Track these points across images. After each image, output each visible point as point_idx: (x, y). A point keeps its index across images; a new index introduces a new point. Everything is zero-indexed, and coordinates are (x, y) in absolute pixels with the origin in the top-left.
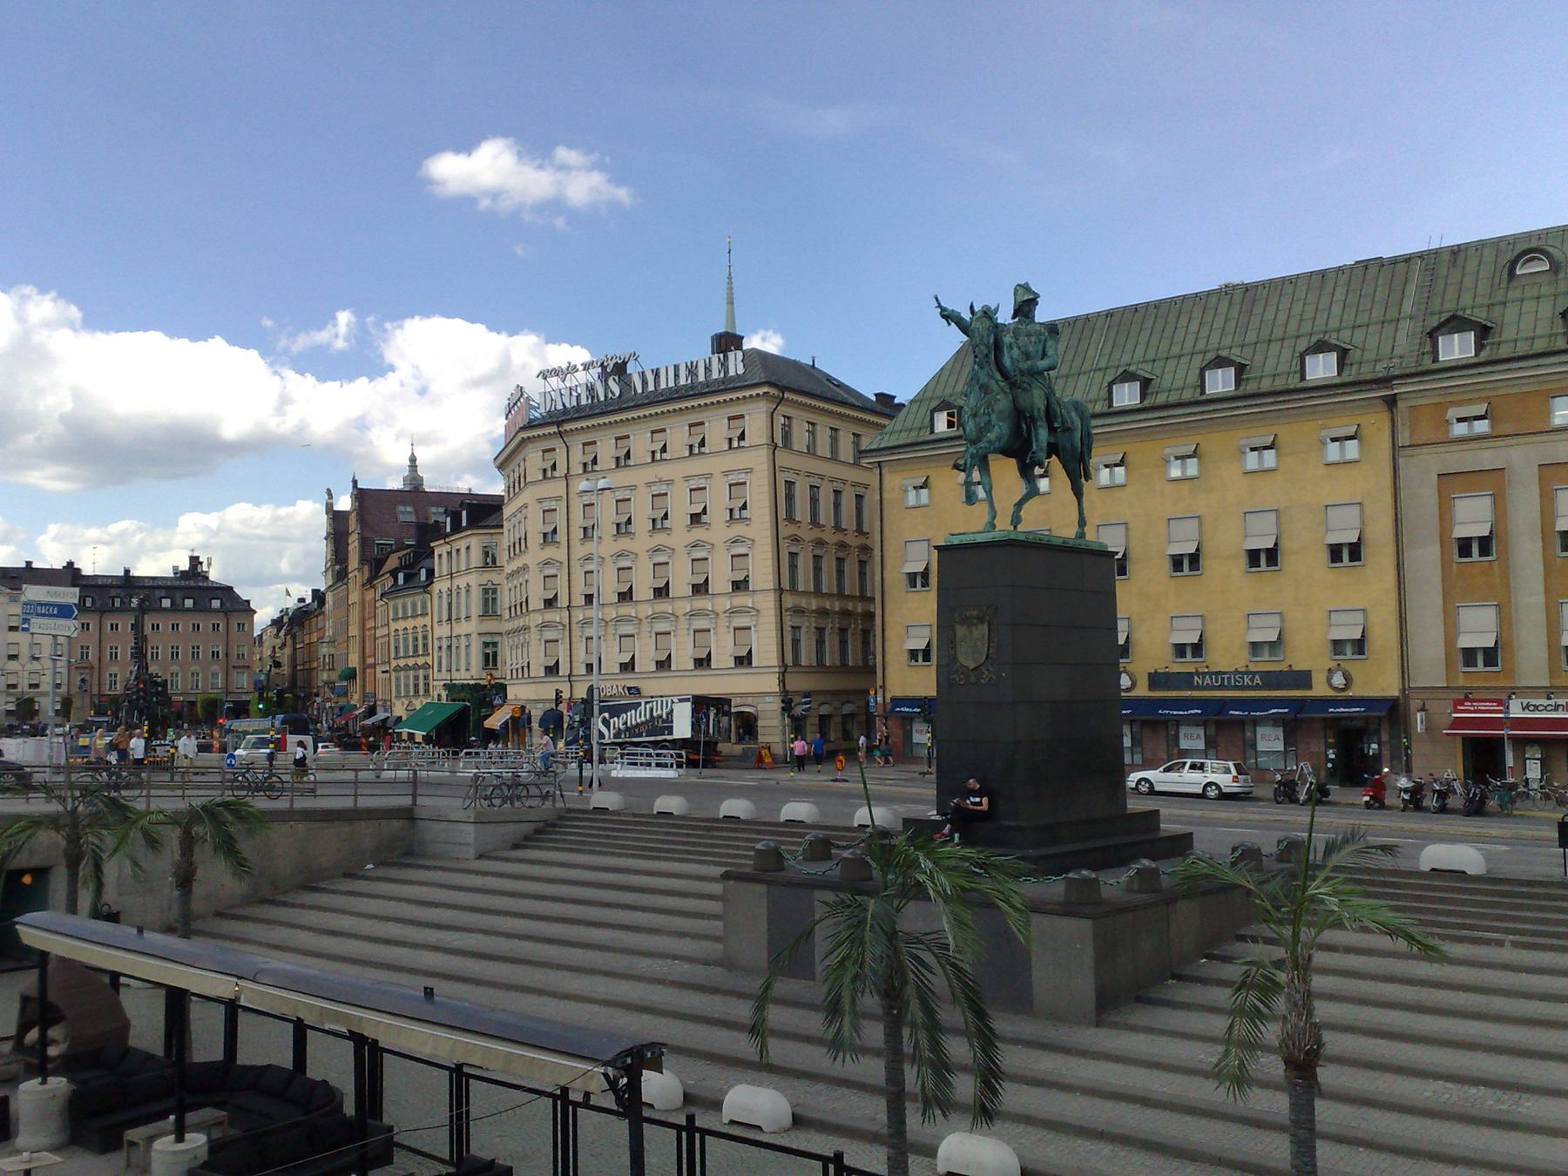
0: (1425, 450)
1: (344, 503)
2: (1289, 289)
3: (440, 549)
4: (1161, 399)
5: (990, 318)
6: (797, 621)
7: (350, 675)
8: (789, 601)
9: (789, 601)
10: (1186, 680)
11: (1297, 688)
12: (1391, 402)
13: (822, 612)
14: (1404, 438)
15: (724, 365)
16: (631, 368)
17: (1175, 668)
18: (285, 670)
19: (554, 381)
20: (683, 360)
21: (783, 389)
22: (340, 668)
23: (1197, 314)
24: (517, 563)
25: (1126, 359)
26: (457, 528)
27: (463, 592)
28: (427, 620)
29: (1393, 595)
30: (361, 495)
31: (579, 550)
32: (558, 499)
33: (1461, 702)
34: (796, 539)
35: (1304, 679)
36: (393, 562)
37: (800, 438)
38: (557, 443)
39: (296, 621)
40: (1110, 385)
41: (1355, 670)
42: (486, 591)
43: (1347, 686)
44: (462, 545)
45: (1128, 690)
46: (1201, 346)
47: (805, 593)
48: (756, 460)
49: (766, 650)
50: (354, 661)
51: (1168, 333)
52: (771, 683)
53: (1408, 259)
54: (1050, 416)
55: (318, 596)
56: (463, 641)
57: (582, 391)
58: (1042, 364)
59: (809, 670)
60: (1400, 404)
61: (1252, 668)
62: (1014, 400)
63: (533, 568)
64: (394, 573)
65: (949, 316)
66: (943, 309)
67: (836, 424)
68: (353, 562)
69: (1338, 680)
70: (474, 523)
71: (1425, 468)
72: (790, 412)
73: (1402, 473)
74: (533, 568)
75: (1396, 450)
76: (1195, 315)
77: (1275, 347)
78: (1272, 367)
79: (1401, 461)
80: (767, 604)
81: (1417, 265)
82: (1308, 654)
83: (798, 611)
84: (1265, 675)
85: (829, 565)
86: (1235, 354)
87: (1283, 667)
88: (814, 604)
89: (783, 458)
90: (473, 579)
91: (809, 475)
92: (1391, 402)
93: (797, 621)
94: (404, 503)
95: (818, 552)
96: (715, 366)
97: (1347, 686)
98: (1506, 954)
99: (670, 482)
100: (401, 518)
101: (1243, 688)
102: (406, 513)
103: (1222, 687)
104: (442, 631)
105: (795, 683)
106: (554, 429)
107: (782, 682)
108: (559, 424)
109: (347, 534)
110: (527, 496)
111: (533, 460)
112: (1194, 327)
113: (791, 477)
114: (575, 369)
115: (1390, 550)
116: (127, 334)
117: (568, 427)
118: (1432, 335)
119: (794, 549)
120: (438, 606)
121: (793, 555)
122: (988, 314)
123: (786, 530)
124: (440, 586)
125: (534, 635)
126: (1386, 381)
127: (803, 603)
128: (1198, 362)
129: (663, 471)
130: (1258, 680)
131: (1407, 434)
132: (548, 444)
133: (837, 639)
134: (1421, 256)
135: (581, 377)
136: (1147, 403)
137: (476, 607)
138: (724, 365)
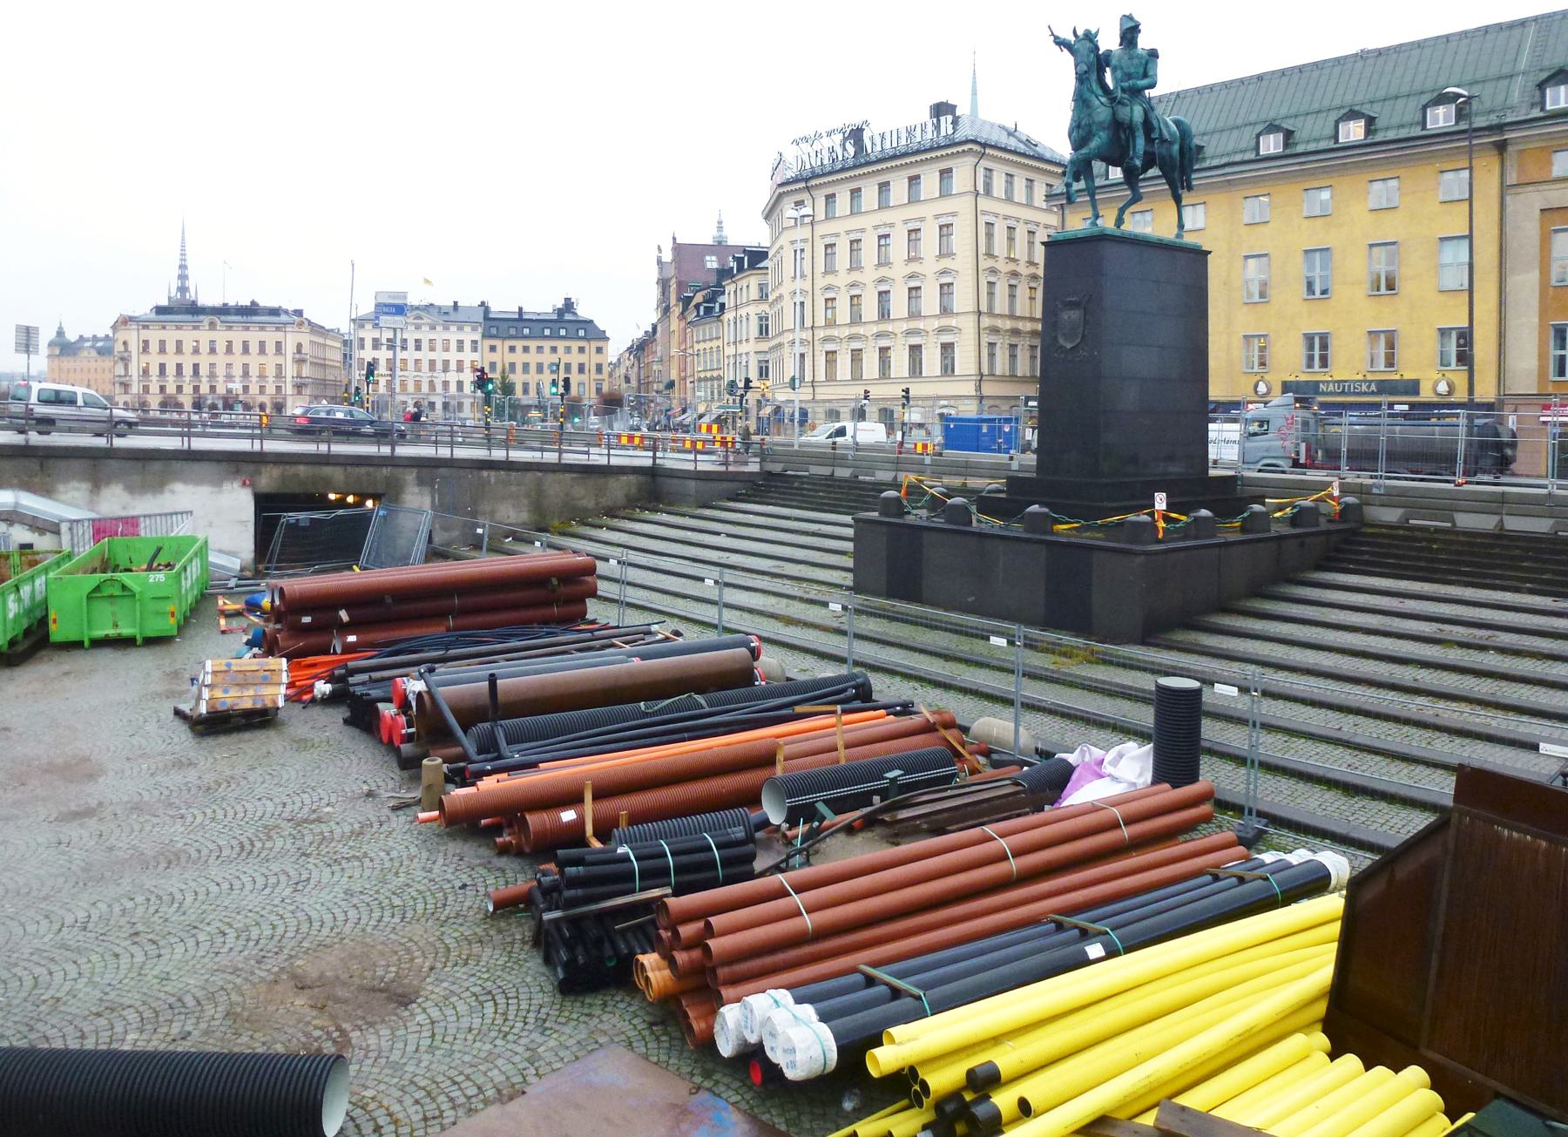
0: (1530, 188)
1: (667, 256)
2: (1416, 52)
3: (730, 288)
4: (1300, 149)
5: (1091, 41)
6: (992, 339)
7: (671, 385)
8: (986, 322)
9: (986, 322)
12: (1501, 147)
13: (1015, 332)
14: (1512, 178)
15: (937, 127)
16: (866, 135)
17: (1303, 378)
18: (634, 383)
19: (805, 147)
20: (902, 124)
21: (984, 145)
22: (666, 381)
24: (776, 294)
26: (741, 269)
28: (720, 343)
29: (1495, 315)
30: (678, 248)
31: (821, 282)
32: (804, 241)
34: (993, 271)
36: (699, 298)
37: (1020, 193)
38: (805, 196)
39: (640, 348)
40: (1258, 137)
42: (761, 319)
44: (744, 283)
46: (1337, 102)
47: (1001, 316)
48: (962, 206)
49: (965, 361)
50: (674, 375)
52: (969, 389)
53: (1523, 23)
54: (1148, 125)
55: (655, 328)
56: (744, 359)
57: (826, 154)
58: (1141, 83)
59: (1002, 379)
60: (1510, 149)
61: (1369, 377)
62: (1114, 114)
63: (787, 297)
64: (697, 307)
65: (1060, 43)
66: (1056, 38)
67: (1031, 176)
68: (673, 301)
70: (752, 266)
71: (1527, 206)
72: (990, 165)
73: (1509, 210)
74: (787, 297)
75: (1504, 189)
78: (1396, 119)
79: (1508, 199)
80: (968, 325)
81: (1532, 29)
83: (995, 330)
84: (1380, 383)
85: (1001, 290)
86: (1366, 110)
87: (1397, 377)
88: (1008, 324)
89: (984, 204)
90: (753, 310)
91: (1006, 218)
92: (1501, 147)
93: (992, 339)
94: (712, 254)
95: (1013, 282)
96: (930, 128)
97: (1450, 393)
98: (664, 517)
99: (892, 225)
100: (709, 265)
101: (1355, 394)
102: (712, 263)
103: (1343, 393)
104: (730, 351)
105: (989, 389)
106: (803, 185)
107: (979, 388)
108: (807, 180)
110: (784, 240)
111: (789, 211)
113: (991, 219)
114: (821, 136)
115: (1494, 276)
117: (813, 182)
118: (1541, 86)
119: (992, 279)
120: (729, 334)
121: (991, 284)
122: (1089, 37)
123: (985, 263)
124: (729, 316)
125: (787, 349)
126: (1500, 128)
127: (999, 323)
128: (1334, 116)
129: (887, 216)
130: (1373, 388)
131: (1514, 176)
132: (798, 197)
133: (1028, 354)
134: (1536, 19)
135: (827, 142)
136: (1288, 152)
137: (754, 332)
138: (937, 127)
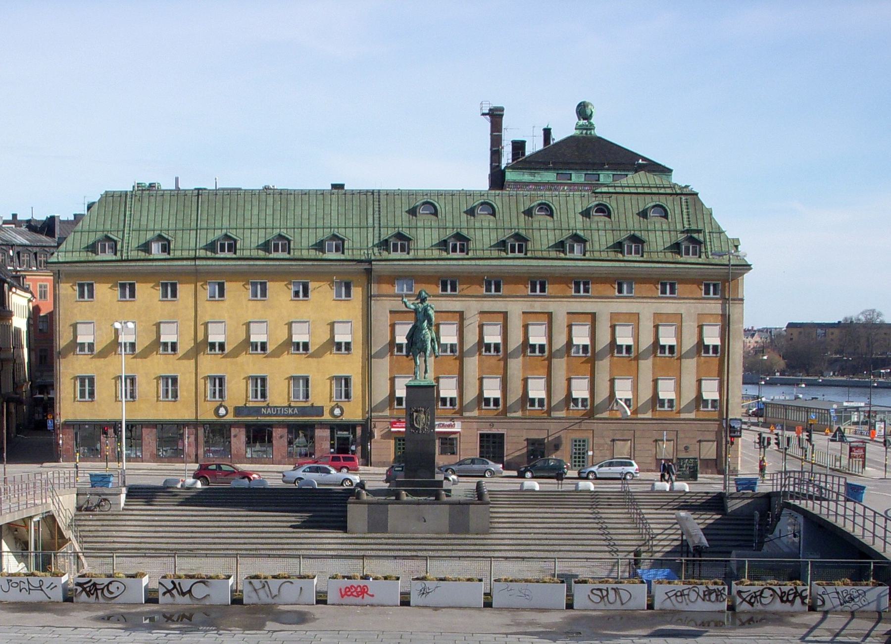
10: (257, 411)
11: (317, 416)
23: (256, 203)
25: (226, 224)
27: (750, 532)
33: (395, 423)
35: (320, 411)
41: (345, 406)
43: (342, 414)
45: (224, 416)
51: (240, 212)
69: (337, 412)
76: (254, 203)
77: (305, 232)
82: (321, 395)
101: (288, 415)
109: (693, 476)
112: (255, 212)
116: (488, 172)
130: (296, 411)
